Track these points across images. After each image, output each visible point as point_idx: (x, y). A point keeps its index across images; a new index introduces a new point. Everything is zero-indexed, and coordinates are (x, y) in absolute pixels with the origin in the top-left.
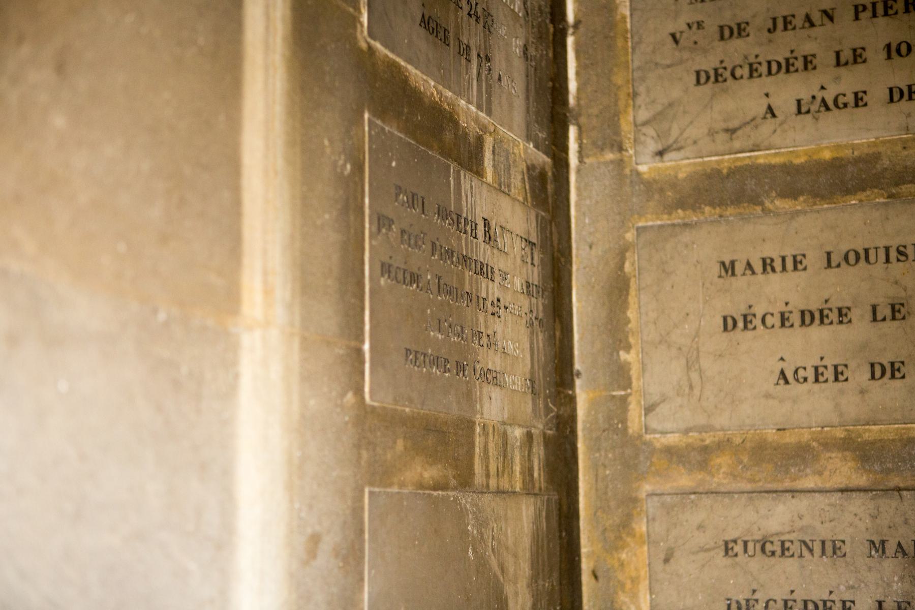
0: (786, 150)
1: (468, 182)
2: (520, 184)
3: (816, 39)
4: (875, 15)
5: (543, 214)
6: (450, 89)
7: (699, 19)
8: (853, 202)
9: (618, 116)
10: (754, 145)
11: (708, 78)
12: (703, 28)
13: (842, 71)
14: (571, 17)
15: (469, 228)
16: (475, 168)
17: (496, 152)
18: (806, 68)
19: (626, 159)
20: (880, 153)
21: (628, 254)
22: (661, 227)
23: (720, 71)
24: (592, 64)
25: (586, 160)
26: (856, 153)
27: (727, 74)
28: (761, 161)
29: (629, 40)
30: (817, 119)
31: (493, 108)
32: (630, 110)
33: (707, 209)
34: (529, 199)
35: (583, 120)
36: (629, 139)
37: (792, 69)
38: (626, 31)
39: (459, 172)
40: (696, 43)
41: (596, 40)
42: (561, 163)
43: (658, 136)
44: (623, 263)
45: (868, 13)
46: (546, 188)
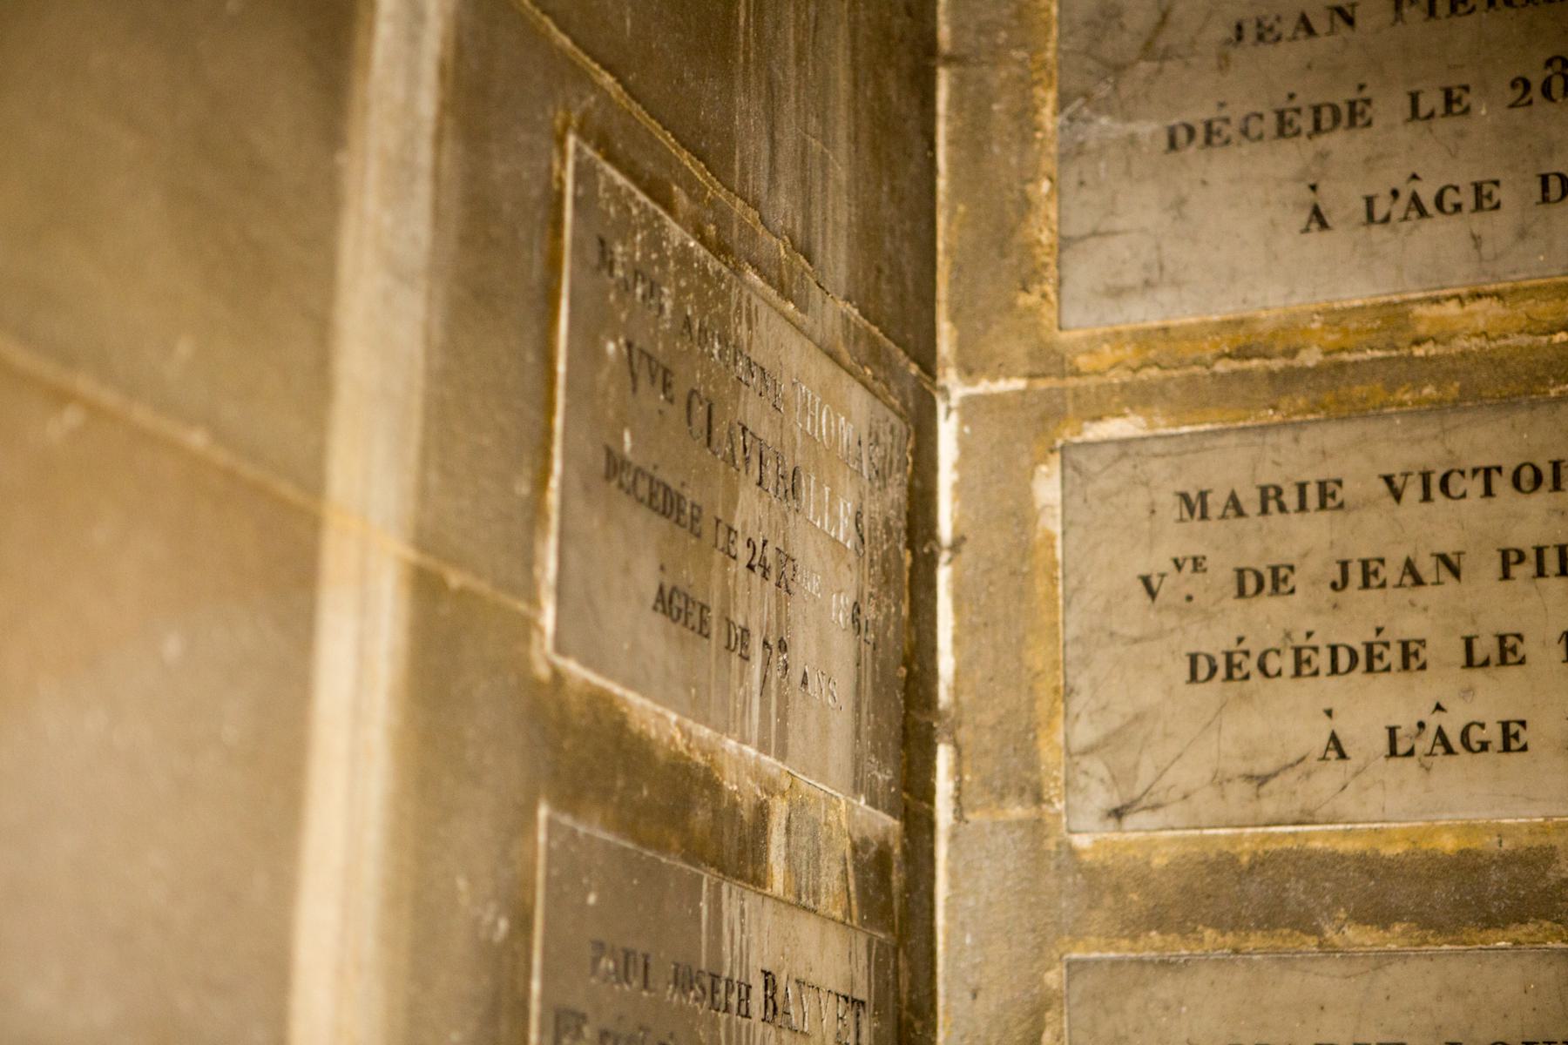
0: (1366, 826)
1: (736, 903)
2: (837, 884)
3: (1425, 609)
4: (1541, 573)
5: (882, 936)
6: (706, 721)
7: (1196, 553)
8: (1502, 944)
9: (1034, 730)
10: (1302, 811)
11: (1213, 670)
12: (1205, 570)
13: (1477, 676)
14: (945, 530)
15: (734, 999)
16: (750, 871)
17: (793, 828)
18: (1406, 666)
19: (1049, 820)
20: (1553, 848)
21: (1049, 1016)
22: (1115, 963)
23: (1237, 658)
24: (986, 625)
25: (969, 816)
26: (1506, 845)
27: (1251, 665)
28: (1317, 844)
29: (1060, 583)
30: (1428, 770)
31: (790, 741)
32: (1059, 720)
33: (1209, 934)
34: (855, 912)
35: (964, 734)
36: (1056, 779)
37: (1378, 665)
38: (1054, 564)
39: (718, 886)
40: (1189, 598)
41: (994, 576)
42: (918, 824)
43: (1113, 777)
44: (1041, 1033)
45: (1529, 568)
46: (889, 881)
